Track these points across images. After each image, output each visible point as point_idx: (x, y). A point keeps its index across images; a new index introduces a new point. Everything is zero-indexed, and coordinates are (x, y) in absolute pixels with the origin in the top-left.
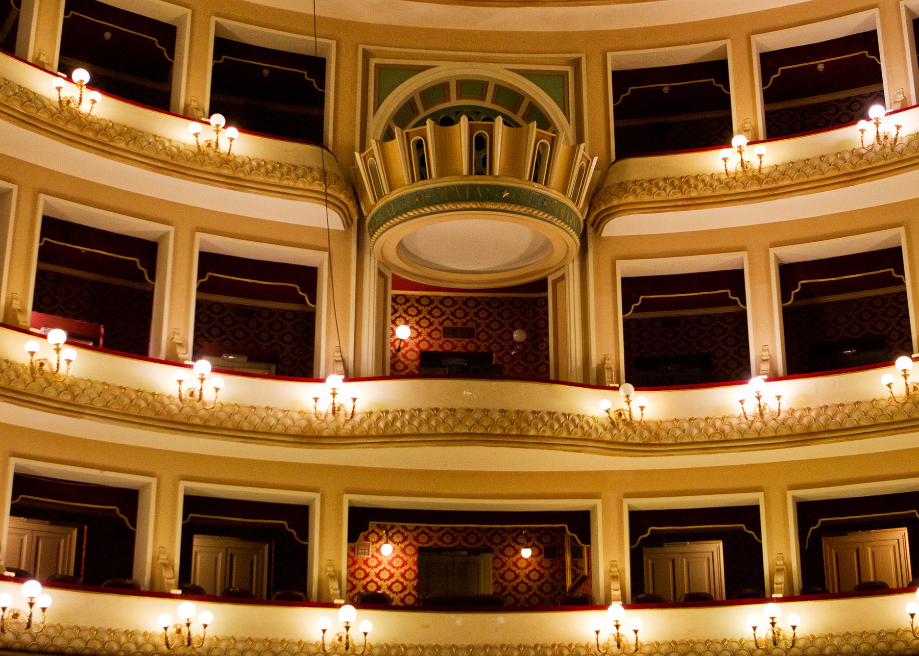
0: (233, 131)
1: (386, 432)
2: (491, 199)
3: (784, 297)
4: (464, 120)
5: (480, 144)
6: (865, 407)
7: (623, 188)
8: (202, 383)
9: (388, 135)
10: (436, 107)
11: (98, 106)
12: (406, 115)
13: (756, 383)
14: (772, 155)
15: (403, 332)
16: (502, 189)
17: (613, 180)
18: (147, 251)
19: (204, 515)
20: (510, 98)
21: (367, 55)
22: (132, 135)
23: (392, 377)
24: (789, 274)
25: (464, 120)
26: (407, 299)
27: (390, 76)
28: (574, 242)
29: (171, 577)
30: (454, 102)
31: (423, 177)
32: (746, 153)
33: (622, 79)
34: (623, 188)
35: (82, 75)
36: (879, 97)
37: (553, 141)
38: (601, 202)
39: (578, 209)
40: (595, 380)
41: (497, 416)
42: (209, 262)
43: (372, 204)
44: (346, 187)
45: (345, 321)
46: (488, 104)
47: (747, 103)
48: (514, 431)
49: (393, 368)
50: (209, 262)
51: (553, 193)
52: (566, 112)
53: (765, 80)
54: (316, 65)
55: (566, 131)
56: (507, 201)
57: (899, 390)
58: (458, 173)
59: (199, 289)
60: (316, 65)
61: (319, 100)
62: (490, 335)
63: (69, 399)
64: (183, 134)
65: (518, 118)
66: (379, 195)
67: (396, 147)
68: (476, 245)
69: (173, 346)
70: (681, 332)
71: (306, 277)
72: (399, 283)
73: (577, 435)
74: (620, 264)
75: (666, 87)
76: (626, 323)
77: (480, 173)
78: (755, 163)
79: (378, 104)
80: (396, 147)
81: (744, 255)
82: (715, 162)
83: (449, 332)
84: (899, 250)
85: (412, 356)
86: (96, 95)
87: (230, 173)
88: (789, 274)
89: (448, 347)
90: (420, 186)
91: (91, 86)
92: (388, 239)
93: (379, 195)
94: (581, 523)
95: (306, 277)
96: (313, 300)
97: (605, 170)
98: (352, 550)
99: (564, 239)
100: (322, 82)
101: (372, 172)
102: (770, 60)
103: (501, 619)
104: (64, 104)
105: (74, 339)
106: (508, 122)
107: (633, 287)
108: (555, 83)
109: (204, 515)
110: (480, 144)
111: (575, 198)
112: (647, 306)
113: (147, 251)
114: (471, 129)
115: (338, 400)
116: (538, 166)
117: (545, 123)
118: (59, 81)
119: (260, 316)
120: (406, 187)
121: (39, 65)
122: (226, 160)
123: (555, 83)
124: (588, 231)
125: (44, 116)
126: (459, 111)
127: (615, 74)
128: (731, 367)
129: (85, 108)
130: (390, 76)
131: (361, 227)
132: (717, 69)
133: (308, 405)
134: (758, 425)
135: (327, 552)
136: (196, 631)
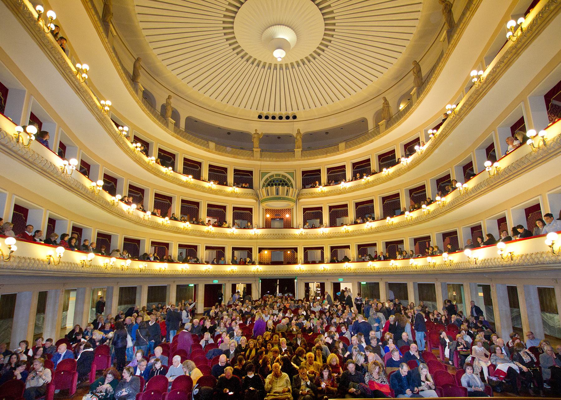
1: (263, 237)
8: (234, 231)
10: (271, 183)
15: (268, 216)
17: (301, 193)
19: (237, 172)
21: (260, 171)
27: (263, 174)
29: (230, 261)
38: (299, 196)
40: (298, 228)
42: (235, 170)
44: (257, 197)
45: (258, 218)
48: (284, 237)
50: (235, 170)
51: (290, 197)
62: (278, 221)
63: (213, 236)
64: (229, 189)
70: (312, 216)
71: (251, 210)
73: (294, 237)
83: (276, 215)
90: (268, 197)
94: (296, 249)
95: (251, 210)
97: (300, 191)
98: (259, 252)
101: (260, 193)
103: (282, 266)
105: (193, 178)
108: (292, 174)
109: (237, 172)
119: (243, 216)
122: (236, 194)
123: (292, 174)
130: (263, 174)
133: (251, 233)
135: (255, 255)
136: (234, 270)
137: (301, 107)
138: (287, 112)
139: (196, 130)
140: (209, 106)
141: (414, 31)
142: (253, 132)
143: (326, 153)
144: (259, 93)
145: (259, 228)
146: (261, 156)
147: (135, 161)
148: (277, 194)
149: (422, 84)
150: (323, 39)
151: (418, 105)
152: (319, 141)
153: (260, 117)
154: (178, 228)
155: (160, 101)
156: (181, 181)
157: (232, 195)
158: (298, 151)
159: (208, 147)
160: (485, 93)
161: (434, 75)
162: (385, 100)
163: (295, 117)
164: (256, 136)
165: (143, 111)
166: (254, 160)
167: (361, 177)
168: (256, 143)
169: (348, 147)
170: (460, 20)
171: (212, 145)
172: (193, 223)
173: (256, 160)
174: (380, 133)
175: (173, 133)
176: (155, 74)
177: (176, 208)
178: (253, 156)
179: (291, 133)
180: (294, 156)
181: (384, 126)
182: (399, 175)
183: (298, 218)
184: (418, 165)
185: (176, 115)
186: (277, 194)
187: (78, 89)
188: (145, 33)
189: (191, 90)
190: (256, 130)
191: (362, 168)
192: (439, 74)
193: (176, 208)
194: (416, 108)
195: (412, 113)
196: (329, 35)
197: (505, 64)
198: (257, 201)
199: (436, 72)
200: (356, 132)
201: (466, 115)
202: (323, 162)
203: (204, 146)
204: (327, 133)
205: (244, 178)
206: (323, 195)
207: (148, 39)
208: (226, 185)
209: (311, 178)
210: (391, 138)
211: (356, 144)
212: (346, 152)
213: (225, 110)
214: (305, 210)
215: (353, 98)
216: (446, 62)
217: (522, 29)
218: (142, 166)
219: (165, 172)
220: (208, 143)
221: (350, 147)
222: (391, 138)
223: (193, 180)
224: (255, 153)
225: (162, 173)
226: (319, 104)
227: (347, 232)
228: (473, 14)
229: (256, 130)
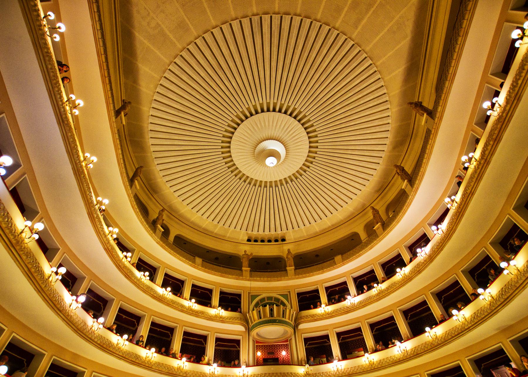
0: (223, 310)
2: (276, 322)
3: (339, 340)
4: (268, 306)
5: (271, 310)
6: (361, 367)
7: (301, 318)
9: (253, 310)
10: (263, 303)
11: (197, 307)
12: (257, 305)
13: (335, 362)
14: (331, 308)
16: (276, 320)
17: (299, 316)
18: (205, 338)
20: (277, 300)
22: (202, 313)
23: (257, 365)
24: (339, 335)
25: (268, 306)
26: (260, 346)
27: (253, 297)
28: (292, 331)
30: (266, 302)
31: (260, 318)
32: (324, 309)
33: (299, 294)
34: (301, 318)
35: (193, 300)
36: (349, 294)
37: (286, 309)
39: (292, 323)
40: (300, 364)
41: (279, 374)
43: (251, 325)
44: (245, 321)
45: (246, 353)
46: (273, 301)
47: (324, 298)
49: (257, 363)
50: (186, 333)
51: (287, 320)
52: (288, 302)
53: (327, 293)
54: (239, 296)
55: (289, 306)
56: (278, 322)
57: (349, 304)
58: (267, 317)
59: (216, 346)
60: (239, 296)
61: (240, 303)
65: (279, 304)
66: (252, 323)
67: (255, 312)
68: (271, 332)
69: (209, 360)
71: (238, 342)
72: (257, 342)
74: (303, 335)
75: (308, 295)
76: (306, 349)
77: (272, 317)
78: (327, 311)
79: (251, 303)
80: (255, 312)
81: (328, 331)
82: (319, 311)
83: (269, 353)
84: (360, 328)
85: (261, 359)
86: (196, 304)
87: (222, 320)
88: (339, 335)
89: (269, 357)
91: (195, 303)
92: (254, 333)
93: (252, 323)
95: (238, 342)
96: (239, 347)
99: (290, 330)
100: (240, 299)
101: (250, 317)
102: (327, 289)
104: (189, 307)
105: (189, 360)
106: (276, 306)
107: (306, 340)
108: (285, 296)
110: (271, 310)
111: (292, 321)
112: (310, 344)
113: (205, 338)
114: (269, 307)
115: (369, 359)
116: (283, 314)
117: (284, 305)
118: (189, 302)
120: (257, 321)
121: (185, 299)
123: (285, 296)
124: (295, 327)
125: (185, 310)
126: (267, 303)
127: (297, 294)
128: (330, 359)
129: (193, 308)
130: (253, 297)
131: (249, 330)
132: (317, 291)
134: (338, 373)
137: (290, 226)
138: (277, 232)
139: (184, 247)
140: (200, 227)
141: (387, 142)
142: (242, 253)
143: (322, 269)
144: (249, 212)
145: (248, 366)
146: (251, 276)
147: (105, 249)
148: (272, 314)
149: (412, 178)
150: (304, 165)
151: (415, 194)
152: (308, 261)
153: (249, 240)
154: (137, 357)
155: (154, 215)
156: (155, 292)
157: (216, 322)
158: (291, 269)
159: (194, 262)
160: (511, 116)
161: (426, 156)
162: (373, 208)
163: (283, 240)
164: (245, 256)
165: (133, 207)
166: (243, 279)
167: (370, 288)
168: (245, 263)
169: (345, 260)
170: (437, 103)
171: (199, 260)
172: (162, 354)
173: (246, 280)
174: (378, 237)
175: (159, 240)
176: (152, 189)
177: (144, 331)
178: (242, 275)
179: (281, 254)
180: (287, 276)
181: (381, 229)
182: (419, 272)
183: (301, 352)
184: (442, 250)
185: (166, 233)
186: (272, 314)
187: (78, 171)
188: (153, 149)
189: (185, 209)
190: (245, 251)
191: (365, 281)
192: (431, 153)
193: (144, 331)
194: (414, 198)
195: (410, 204)
196: (311, 157)
197: (495, 139)
198: (246, 330)
199: (427, 151)
200: (349, 246)
201: (493, 154)
202: (321, 278)
203: (190, 260)
204: (317, 256)
205: (230, 301)
206: (326, 319)
207: (154, 155)
208: (211, 307)
209: (309, 300)
210: (392, 239)
211: (353, 255)
212: (344, 264)
213: (215, 231)
214: (306, 340)
215: (339, 215)
216: (435, 138)
217: (456, 202)
218: (112, 260)
219: (139, 277)
220: (194, 259)
221: (348, 258)
222: (392, 239)
223: (187, 364)
224: (244, 272)
225: (136, 278)
226: (307, 224)
227: (371, 364)
228: (452, 83)
229: (245, 251)
